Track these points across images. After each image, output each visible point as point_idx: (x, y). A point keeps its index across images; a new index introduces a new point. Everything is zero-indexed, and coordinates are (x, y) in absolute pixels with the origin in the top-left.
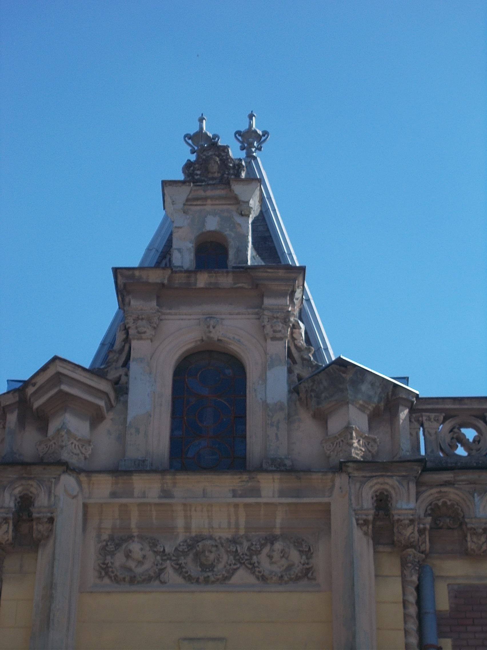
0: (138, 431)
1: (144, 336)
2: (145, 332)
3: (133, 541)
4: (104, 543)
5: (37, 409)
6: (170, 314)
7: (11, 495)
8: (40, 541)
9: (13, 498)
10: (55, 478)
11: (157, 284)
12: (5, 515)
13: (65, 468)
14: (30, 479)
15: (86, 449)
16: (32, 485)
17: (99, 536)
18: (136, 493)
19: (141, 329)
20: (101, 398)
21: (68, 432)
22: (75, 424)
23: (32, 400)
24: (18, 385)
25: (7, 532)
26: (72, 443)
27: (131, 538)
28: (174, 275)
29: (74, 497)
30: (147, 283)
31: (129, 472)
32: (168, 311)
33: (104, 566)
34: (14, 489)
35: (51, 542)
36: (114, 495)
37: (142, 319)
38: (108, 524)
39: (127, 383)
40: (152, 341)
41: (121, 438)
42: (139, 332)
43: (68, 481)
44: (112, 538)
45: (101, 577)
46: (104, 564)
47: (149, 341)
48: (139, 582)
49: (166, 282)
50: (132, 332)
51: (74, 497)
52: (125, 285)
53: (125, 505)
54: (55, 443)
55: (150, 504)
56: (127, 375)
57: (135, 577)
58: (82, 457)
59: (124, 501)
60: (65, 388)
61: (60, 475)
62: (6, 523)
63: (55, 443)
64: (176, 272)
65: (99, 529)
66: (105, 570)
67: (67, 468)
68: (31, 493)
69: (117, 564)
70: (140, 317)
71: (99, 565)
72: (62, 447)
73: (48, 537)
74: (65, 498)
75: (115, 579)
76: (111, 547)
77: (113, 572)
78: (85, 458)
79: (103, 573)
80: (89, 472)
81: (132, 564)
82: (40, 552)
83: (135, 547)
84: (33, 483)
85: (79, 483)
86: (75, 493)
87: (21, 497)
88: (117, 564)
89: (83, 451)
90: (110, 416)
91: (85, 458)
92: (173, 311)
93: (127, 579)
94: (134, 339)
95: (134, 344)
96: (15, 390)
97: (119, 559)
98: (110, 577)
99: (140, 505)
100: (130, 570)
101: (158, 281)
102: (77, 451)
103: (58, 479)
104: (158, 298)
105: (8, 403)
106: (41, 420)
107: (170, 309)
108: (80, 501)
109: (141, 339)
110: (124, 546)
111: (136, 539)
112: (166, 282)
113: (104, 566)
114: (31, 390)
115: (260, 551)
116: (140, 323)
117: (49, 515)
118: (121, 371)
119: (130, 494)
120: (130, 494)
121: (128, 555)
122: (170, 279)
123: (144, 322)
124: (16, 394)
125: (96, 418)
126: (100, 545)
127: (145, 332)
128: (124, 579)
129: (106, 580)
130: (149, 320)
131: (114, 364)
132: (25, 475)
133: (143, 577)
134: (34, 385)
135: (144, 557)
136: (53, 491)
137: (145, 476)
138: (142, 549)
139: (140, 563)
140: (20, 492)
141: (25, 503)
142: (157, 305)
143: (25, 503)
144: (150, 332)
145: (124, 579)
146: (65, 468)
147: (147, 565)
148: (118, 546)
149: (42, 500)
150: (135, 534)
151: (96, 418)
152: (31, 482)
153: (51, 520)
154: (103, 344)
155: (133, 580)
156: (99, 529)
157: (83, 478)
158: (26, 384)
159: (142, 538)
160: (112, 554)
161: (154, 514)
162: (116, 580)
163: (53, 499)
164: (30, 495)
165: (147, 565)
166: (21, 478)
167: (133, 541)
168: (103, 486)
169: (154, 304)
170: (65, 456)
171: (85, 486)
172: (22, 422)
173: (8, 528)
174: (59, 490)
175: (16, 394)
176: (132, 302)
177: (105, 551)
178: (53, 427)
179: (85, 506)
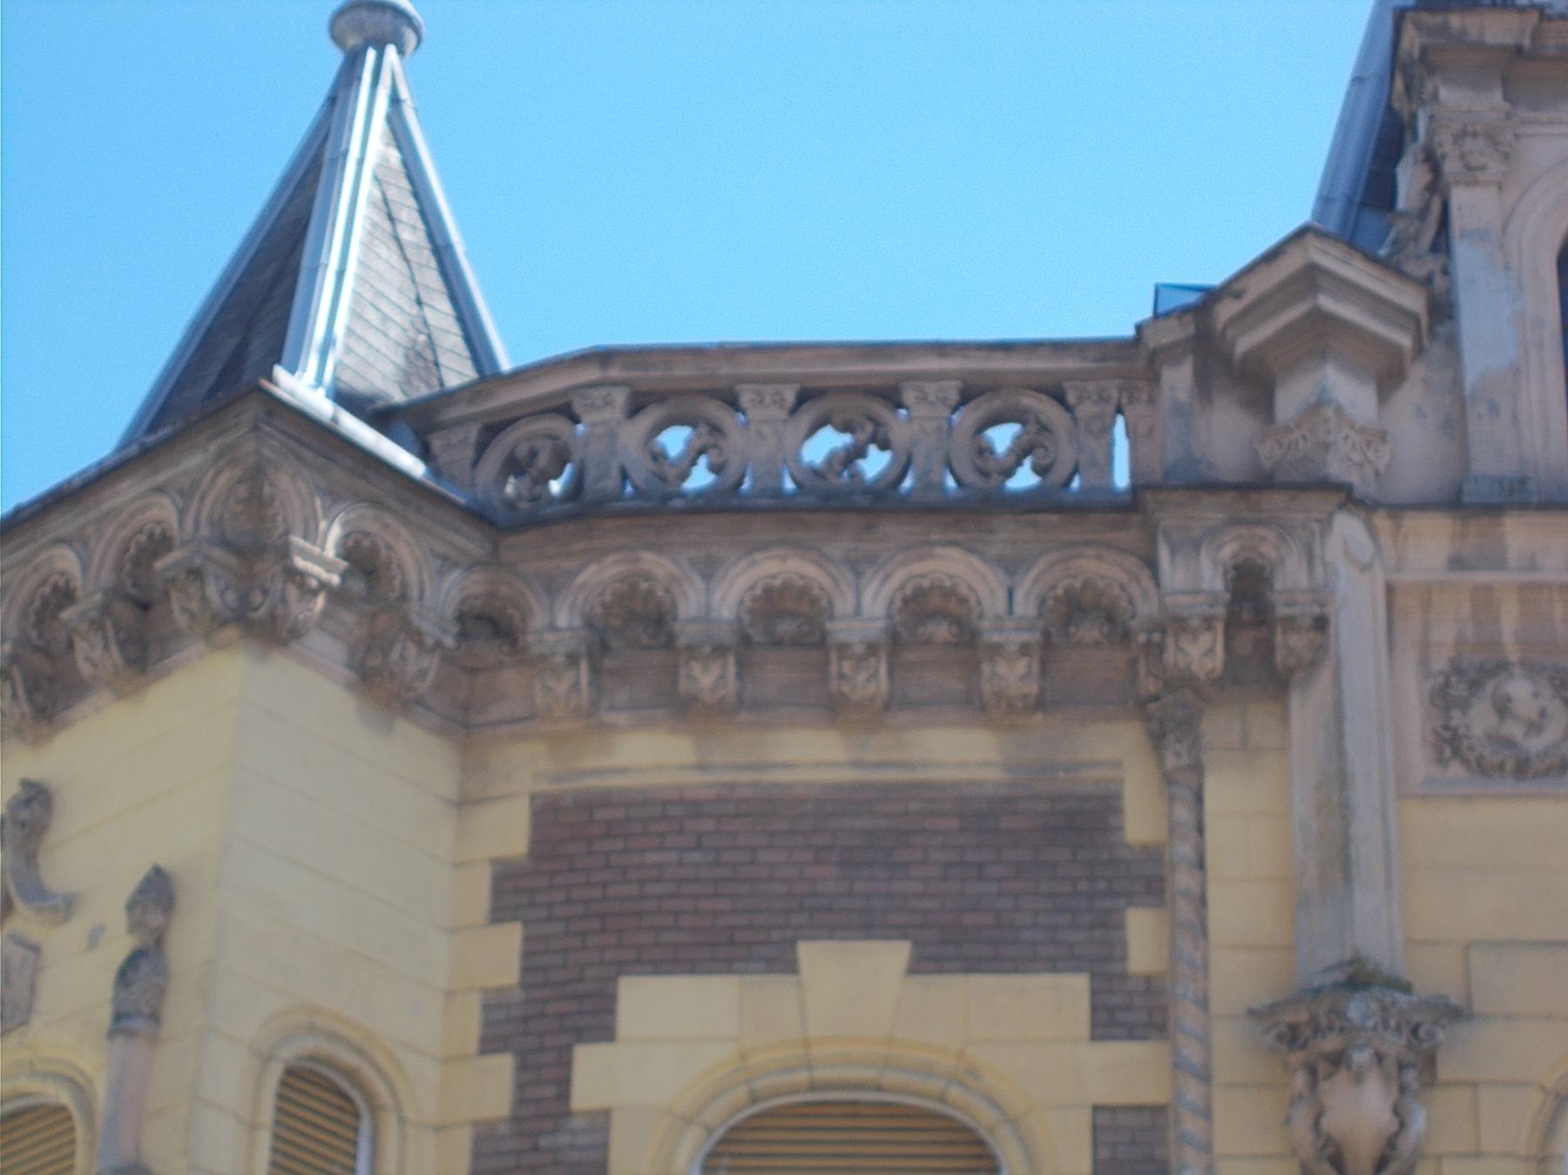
0: (1494, 410)
1: (1481, 176)
2: (1483, 168)
3: (1511, 675)
4: (1441, 680)
5: (1245, 357)
6: (1539, 122)
7: (1215, 563)
8: (1290, 671)
9: (1220, 569)
10: (1319, 521)
11: (1503, 49)
12: (1209, 611)
13: (1341, 497)
14: (1259, 523)
15: (1377, 451)
16: (1263, 539)
17: (1424, 662)
18: (1513, 558)
19: (1475, 160)
20: (1404, 329)
21: (1339, 411)
22: (1351, 393)
23: (1230, 333)
24: (1192, 298)
25: (1211, 650)
26: (1346, 438)
27: (1502, 667)
28: (1545, 25)
29: (1366, 568)
30: (1480, 46)
31: (1493, 509)
32: (1532, 115)
33: (1447, 734)
34: (1219, 548)
35: (1325, 676)
36: (1457, 563)
37: (1475, 135)
38: (1444, 634)
39: (1449, 292)
40: (1500, 187)
41: (1455, 425)
42: (1469, 168)
43: (1348, 526)
44: (1457, 668)
45: (1441, 761)
46: (1446, 728)
47: (1493, 191)
48: (1537, 775)
49: (1527, 43)
50: (1450, 167)
51: (1366, 568)
52: (1424, 51)
53: (1489, 588)
54: (1304, 437)
55: (1549, 586)
56: (1445, 272)
57: (1528, 760)
58: (1369, 470)
59: (1485, 577)
60: (1327, 302)
61: (1331, 515)
62: (1208, 629)
63: (1304, 437)
64: (1550, 19)
65: (1425, 647)
66: (1449, 744)
67: (1348, 497)
68: (1262, 556)
69: (1478, 730)
70: (1470, 129)
71: (1435, 731)
72: (1326, 447)
73: (1313, 664)
74: (1344, 568)
75: (1479, 765)
76: (1459, 689)
77: (1471, 748)
78: (1377, 474)
79: (1448, 751)
80: (1397, 509)
81: (1514, 730)
82: (1295, 700)
83: (1520, 689)
84: (1270, 535)
85: (1373, 533)
86: (1367, 558)
87: (1236, 567)
88: (1478, 730)
89: (1371, 455)
90: (1416, 372)
91: (1377, 474)
92: (1544, 115)
93: (1509, 765)
94: (1457, 183)
95: (1460, 197)
96: (1185, 310)
97: (1479, 721)
98: (1465, 762)
99: (1525, 589)
100: (1510, 744)
101: (1509, 40)
102: (1357, 457)
103: (1326, 524)
104: (1506, 83)
105: (1165, 341)
106: (1255, 384)
107: (1536, 109)
108: (1379, 577)
109: (1473, 183)
110: (1490, 687)
111: (1517, 670)
112: (1527, 43)
113: (1447, 734)
114: (1226, 311)
115: (1447, 709)
116: (1469, 144)
117: (1316, 610)
118: (1432, 264)
119: (1499, 563)
120: (1499, 563)
121: (1503, 708)
122: (1536, 35)
123: (1480, 142)
124: (1189, 318)
125: (1389, 378)
126: (1429, 685)
127: (1483, 168)
128: (1501, 767)
129: (1456, 769)
130: (1492, 139)
131: (1411, 247)
132: (1246, 514)
133: (1548, 761)
134: (1238, 296)
135: (1543, 713)
136: (1318, 552)
137: (1535, 519)
138: (1536, 695)
139: (1535, 727)
140: (1234, 556)
141: (1249, 587)
142: (1506, 98)
143: (1249, 587)
144: (1495, 168)
145: (1501, 767)
146: (1341, 497)
147: (1551, 735)
148: (1475, 686)
149: (1291, 577)
150: (1513, 655)
151: (1388, 377)
152: (1261, 531)
153: (1321, 624)
154: (285, 181)
155: (1522, 769)
156: (1425, 647)
157: (1381, 521)
158: (1211, 297)
159: (1531, 668)
160: (1465, 706)
161: (1558, 610)
162: (1481, 768)
163: (1319, 571)
164: (1260, 561)
165: (1551, 735)
166: (1236, 521)
167: (1511, 675)
168: (1430, 543)
169: (1497, 96)
170: (1335, 469)
171: (1386, 540)
172: (1203, 385)
173: (1214, 642)
174: (1333, 550)
175: (1189, 318)
176: (1444, 93)
177: (1443, 699)
178: (1290, 400)
179: (1390, 589)
